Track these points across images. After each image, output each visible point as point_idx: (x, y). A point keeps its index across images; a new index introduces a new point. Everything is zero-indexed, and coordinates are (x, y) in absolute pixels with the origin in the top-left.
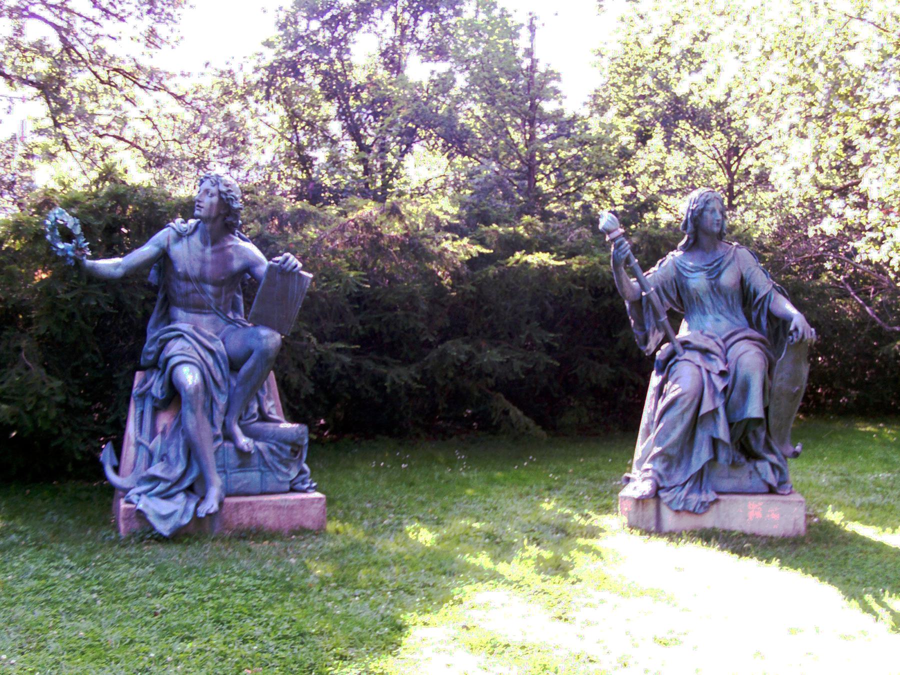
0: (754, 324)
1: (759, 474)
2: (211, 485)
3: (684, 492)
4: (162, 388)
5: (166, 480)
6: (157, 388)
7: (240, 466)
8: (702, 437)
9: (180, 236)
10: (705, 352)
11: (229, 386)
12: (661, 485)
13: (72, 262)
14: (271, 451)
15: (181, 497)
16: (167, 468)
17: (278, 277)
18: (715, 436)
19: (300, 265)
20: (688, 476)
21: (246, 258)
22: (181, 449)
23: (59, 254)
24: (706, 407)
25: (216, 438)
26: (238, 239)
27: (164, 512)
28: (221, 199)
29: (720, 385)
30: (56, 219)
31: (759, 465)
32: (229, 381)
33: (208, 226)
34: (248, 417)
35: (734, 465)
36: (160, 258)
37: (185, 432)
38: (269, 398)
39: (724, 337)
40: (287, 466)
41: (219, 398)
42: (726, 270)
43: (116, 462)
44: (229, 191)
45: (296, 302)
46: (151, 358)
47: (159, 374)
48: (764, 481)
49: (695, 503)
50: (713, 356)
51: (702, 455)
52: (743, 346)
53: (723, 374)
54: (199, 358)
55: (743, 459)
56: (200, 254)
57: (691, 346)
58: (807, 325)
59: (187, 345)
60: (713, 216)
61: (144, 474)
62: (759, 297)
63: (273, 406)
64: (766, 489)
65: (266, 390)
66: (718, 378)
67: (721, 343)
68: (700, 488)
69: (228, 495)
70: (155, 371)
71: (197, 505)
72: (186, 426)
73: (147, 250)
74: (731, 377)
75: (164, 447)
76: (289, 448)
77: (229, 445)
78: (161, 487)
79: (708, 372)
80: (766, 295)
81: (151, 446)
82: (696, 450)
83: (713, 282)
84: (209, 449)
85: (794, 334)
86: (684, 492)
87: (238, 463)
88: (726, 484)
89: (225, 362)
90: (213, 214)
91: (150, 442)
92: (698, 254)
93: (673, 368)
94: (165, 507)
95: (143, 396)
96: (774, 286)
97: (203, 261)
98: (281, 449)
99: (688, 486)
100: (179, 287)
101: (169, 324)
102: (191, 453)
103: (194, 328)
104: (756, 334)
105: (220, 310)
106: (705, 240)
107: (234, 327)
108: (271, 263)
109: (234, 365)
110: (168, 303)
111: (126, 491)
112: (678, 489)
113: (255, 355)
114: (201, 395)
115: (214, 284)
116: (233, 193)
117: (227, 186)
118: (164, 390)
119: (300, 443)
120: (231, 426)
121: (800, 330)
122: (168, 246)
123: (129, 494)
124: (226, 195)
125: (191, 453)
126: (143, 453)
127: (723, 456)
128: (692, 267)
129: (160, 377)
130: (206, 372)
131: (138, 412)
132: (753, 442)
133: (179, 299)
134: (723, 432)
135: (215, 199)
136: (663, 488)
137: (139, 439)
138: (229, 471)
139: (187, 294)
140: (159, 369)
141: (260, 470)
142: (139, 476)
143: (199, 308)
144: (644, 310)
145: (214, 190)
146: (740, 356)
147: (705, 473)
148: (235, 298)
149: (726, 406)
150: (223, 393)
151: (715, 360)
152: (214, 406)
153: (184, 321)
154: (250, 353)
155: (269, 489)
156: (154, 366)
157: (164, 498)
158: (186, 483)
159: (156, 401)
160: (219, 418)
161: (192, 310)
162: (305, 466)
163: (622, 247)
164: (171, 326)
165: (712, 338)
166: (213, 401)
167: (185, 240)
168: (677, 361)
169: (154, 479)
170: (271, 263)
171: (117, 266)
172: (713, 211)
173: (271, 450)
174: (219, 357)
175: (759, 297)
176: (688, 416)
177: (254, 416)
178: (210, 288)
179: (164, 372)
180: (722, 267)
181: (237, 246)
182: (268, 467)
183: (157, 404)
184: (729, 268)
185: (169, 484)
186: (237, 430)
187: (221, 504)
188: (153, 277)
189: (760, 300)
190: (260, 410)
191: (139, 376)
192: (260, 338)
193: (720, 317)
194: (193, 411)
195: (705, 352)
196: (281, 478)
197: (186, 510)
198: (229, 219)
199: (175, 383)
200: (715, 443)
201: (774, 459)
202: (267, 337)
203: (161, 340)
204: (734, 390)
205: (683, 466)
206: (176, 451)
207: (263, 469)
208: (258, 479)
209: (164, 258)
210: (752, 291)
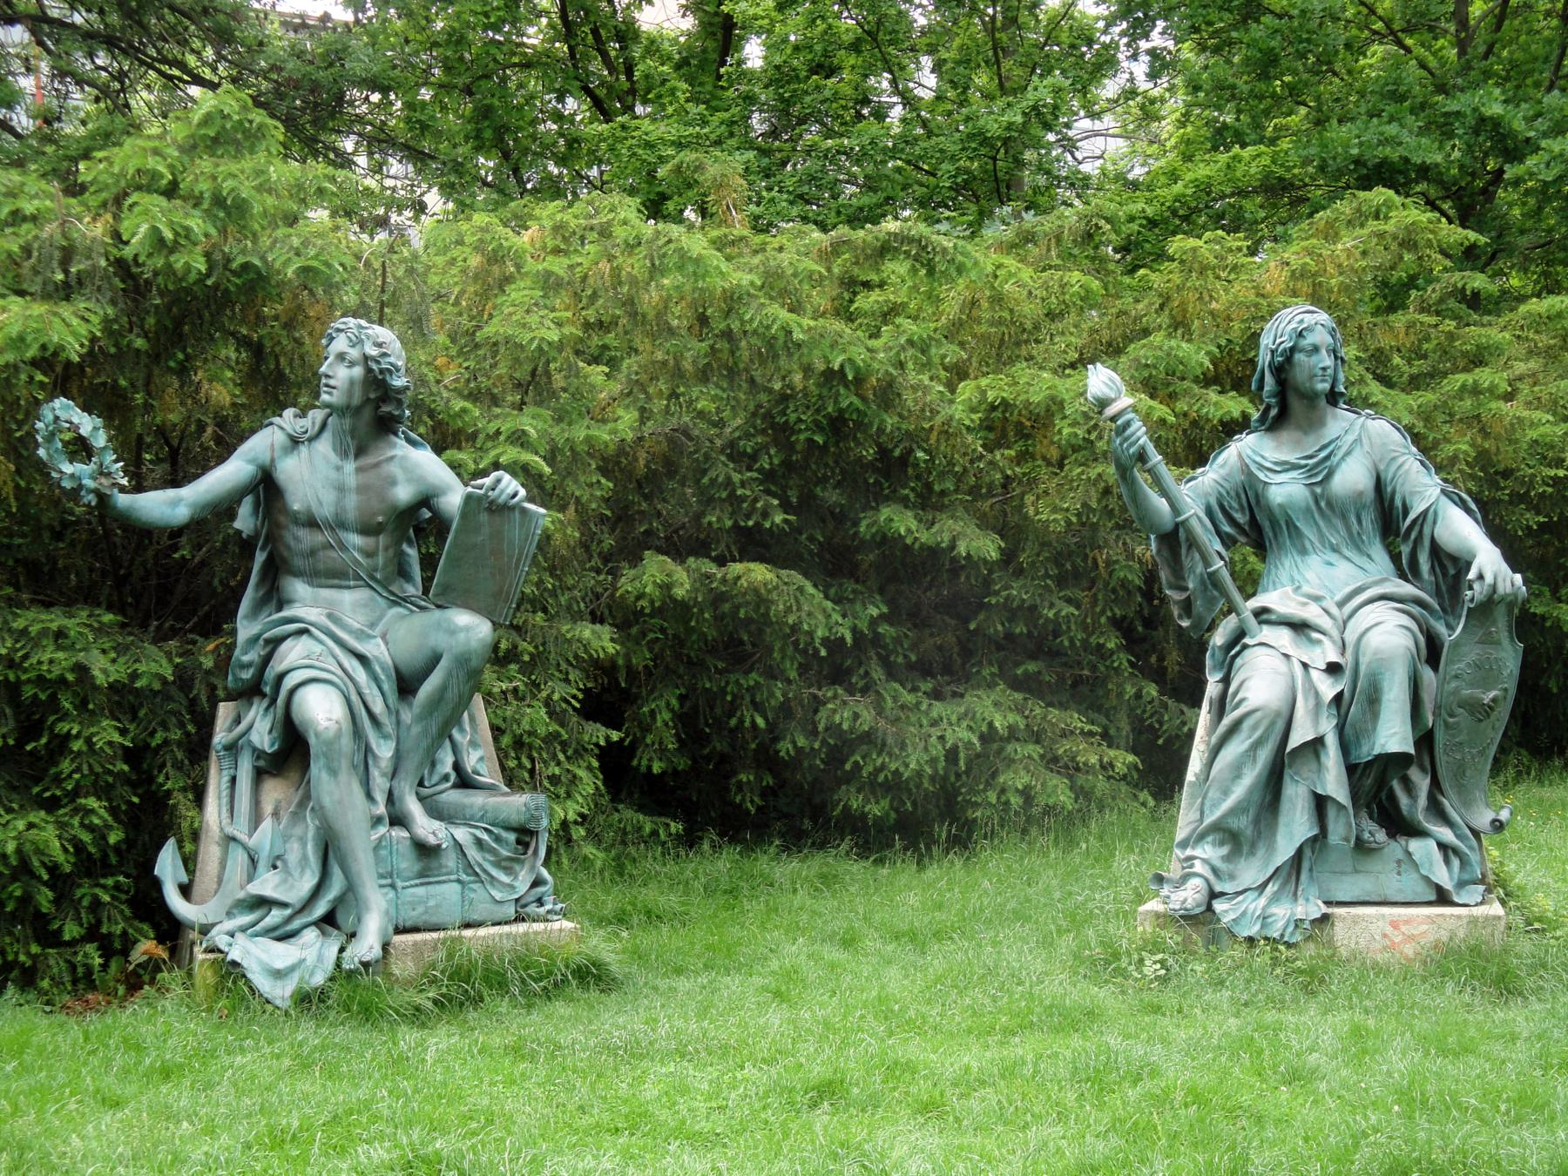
0: (1407, 571)
1: (1416, 866)
2: (368, 909)
3: (1263, 901)
4: (270, 732)
5: (284, 905)
6: (261, 730)
7: (421, 875)
8: (1296, 796)
9: (295, 442)
10: (1300, 627)
11: (398, 723)
12: (1218, 888)
13: (91, 499)
14: (479, 843)
15: (311, 935)
16: (285, 881)
17: (484, 517)
18: (1319, 791)
19: (522, 492)
20: (1271, 870)
21: (420, 479)
22: (310, 847)
23: (67, 484)
24: (1295, 740)
25: (377, 821)
26: (403, 442)
27: (280, 964)
28: (369, 370)
29: (1328, 688)
30: (57, 418)
31: (1415, 845)
32: (397, 712)
33: (347, 422)
34: (435, 779)
35: (1362, 848)
36: (257, 486)
37: (319, 812)
38: (474, 744)
39: (1338, 597)
40: (508, 870)
41: (379, 746)
42: (1344, 465)
43: (185, 878)
44: (385, 355)
45: (519, 560)
46: (247, 675)
47: (265, 703)
48: (1427, 880)
49: (1280, 924)
50: (1315, 635)
51: (1295, 826)
52: (1382, 611)
53: (1333, 669)
54: (340, 672)
55: (1381, 836)
56: (333, 475)
57: (1273, 617)
58: (1505, 567)
59: (318, 648)
60: (1314, 359)
61: (241, 895)
62: (1412, 516)
63: (481, 759)
64: (1433, 897)
65: (468, 728)
66: (1324, 676)
67: (1335, 611)
68: (1295, 894)
69: (399, 931)
70: (256, 700)
71: (342, 950)
72: (318, 801)
73: (232, 472)
74: (1348, 673)
75: (279, 842)
76: (512, 837)
77: (399, 833)
78: (276, 916)
79: (1305, 666)
80: (1426, 512)
81: (251, 843)
82: (1283, 819)
83: (1318, 490)
84: (363, 841)
85: (1476, 586)
86: (1263, 901)
87: (417, 867)
88: (1346, 888)
89: (388, 677)
90: (356, 401)
91: (250, 836)
92: (1286, 435)
93: (1238, 661)
94: (282, 954)
95: (232, 748)
96: (1443, 491)
97: (341, 489)
98: (498, 839)
99: (1270, 889)
100: (296, 539)
101: (280, 608)
102: (329, 850)
103: (330, 616)
104: (1407, 589)
105: (388, 580)
106: (1295, 404)
107: (406, 612)
108: (470, 489)
109: (406, 685)
110: (276, 570)
111: (205, 930)
112: (1251, 895)
113: (443, 663)
114: (346, 742)
115: (367, 530)
116: (392, 359)
117: (380, 345)
118: (275, 734)
119: (532, 826)
120: (402, 799)
121: (1489, 579)
122: (273, 460)
123: (214, 932)
124: (378, 362)
125: (329, 850)
126: (239, 858)
127: (1338, 830)
128: (1276, 463)
129: (267, 709)
130: (354, 698)
131: (226, 779)
132: (1404, 800)
133: (298, 562)
134: (1334, 783)
135: (358, 371)
136: (1222, 894)
137: (230, 830)
138: (399, 884)
139: (313, 553)
140: (264, 695)
141: (459, 881)
142: (229, 902)
143: (335, 576)
144: (1184, 551)
145: (354, 353)
146: (1367, 630)
147: (1306, 865)
148: (401, 555)
149: (1341, 729)
150: (386, 737)
151: (1319, 642)
152: (370, 762)
153: (307, 601)
154: (435, 659)
155: (476, 917)
156: (251, 691)
157: (280, 939)
158: (320, 909)
159: (258, 758)
160: (380, 784)
161: (323, 581)
162: (545, 873)
163: (1128, 432)
164: (285, 613)
165: (1317, 599)
166: (368, 750)
167: (303, 449)
168: (1245, 647)
169: (262, 903)
170: (470, 489)
171: (175, 503)
172: (1316, 349)
173: (479, 843)
174: (378, 669)
175: (1412, 516)
176: (1265, 755)
177: (446, 778)
178: (355, 539)
179: (273, 701)
180: (1335, 460)
181: (403, 458)
182: (477, 874)
183: (262, 763)
184: (1349, 460)
185: (288, 912)
186: (414, 807)
187: (385, 947)
188: (245, 521)
189: (1414, 522)
190: (457, 767)
191: (225, 711)
192: (453, 631)
193: (1333, 557)
194: (333, 772)
195: (1300, 627)
196: (498, 896)
197: (320, 958)
198: (386, 409)
199: (297, 721)
200: (1321, 803)
201: (1447, 834)
202: (467, 629)
203: (267, 642)
204: (1354, 705)
205: (1261, 852)
206: (302, 851)
207: (464, 877)
208: (456, 898)
209: (266, 486)
210: (1398, 502)
